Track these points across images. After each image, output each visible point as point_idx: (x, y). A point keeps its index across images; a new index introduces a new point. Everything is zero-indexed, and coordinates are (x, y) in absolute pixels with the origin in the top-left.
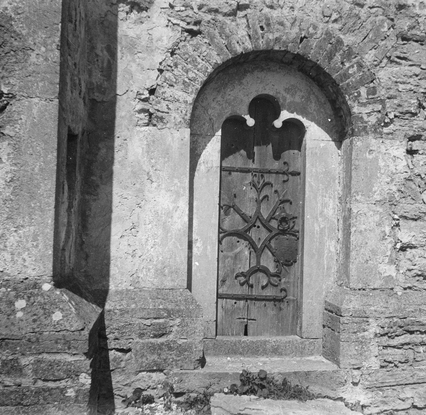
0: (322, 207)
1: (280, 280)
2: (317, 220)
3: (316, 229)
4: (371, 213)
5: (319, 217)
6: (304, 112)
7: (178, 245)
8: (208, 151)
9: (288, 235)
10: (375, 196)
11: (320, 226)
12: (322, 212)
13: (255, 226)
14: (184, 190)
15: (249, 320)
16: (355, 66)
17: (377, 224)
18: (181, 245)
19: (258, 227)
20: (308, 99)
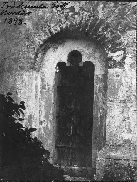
2: (99, 111)
3: (99, 115)
4: (118, 107)
10: (120, 98)
11: (101, 114)
16: (110, 33)
17: (121, 113)
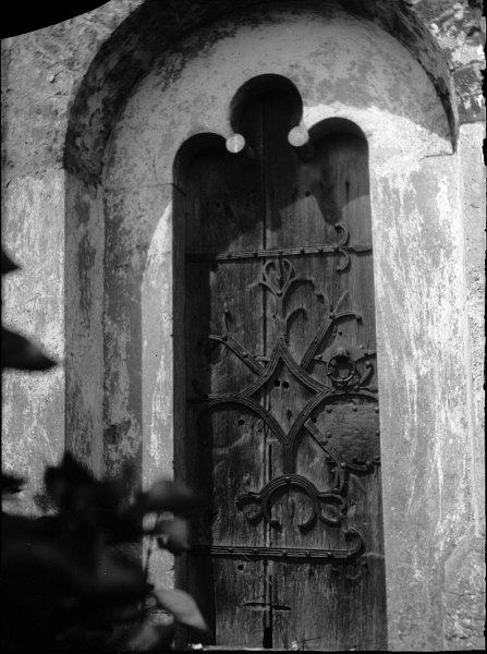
0: (421, 320)
1: (345, 511)
2: (409, 354)
5: (413, 345)
6: (343, 92)
7: (45, 434)
8: (145, 222)
9: (356, 401)
12: (419, 338)
13: (277, 384)
14: (55, 308)
15: (278, 607)
18: (51, 435)
19: (286, 385)
20: (364, 68)
